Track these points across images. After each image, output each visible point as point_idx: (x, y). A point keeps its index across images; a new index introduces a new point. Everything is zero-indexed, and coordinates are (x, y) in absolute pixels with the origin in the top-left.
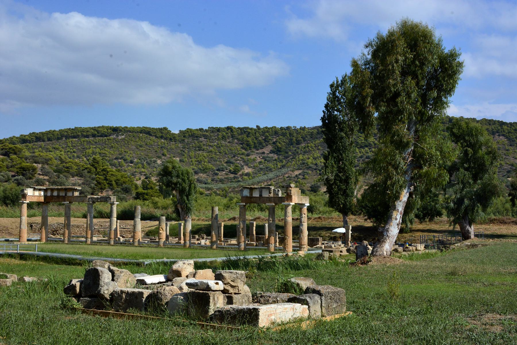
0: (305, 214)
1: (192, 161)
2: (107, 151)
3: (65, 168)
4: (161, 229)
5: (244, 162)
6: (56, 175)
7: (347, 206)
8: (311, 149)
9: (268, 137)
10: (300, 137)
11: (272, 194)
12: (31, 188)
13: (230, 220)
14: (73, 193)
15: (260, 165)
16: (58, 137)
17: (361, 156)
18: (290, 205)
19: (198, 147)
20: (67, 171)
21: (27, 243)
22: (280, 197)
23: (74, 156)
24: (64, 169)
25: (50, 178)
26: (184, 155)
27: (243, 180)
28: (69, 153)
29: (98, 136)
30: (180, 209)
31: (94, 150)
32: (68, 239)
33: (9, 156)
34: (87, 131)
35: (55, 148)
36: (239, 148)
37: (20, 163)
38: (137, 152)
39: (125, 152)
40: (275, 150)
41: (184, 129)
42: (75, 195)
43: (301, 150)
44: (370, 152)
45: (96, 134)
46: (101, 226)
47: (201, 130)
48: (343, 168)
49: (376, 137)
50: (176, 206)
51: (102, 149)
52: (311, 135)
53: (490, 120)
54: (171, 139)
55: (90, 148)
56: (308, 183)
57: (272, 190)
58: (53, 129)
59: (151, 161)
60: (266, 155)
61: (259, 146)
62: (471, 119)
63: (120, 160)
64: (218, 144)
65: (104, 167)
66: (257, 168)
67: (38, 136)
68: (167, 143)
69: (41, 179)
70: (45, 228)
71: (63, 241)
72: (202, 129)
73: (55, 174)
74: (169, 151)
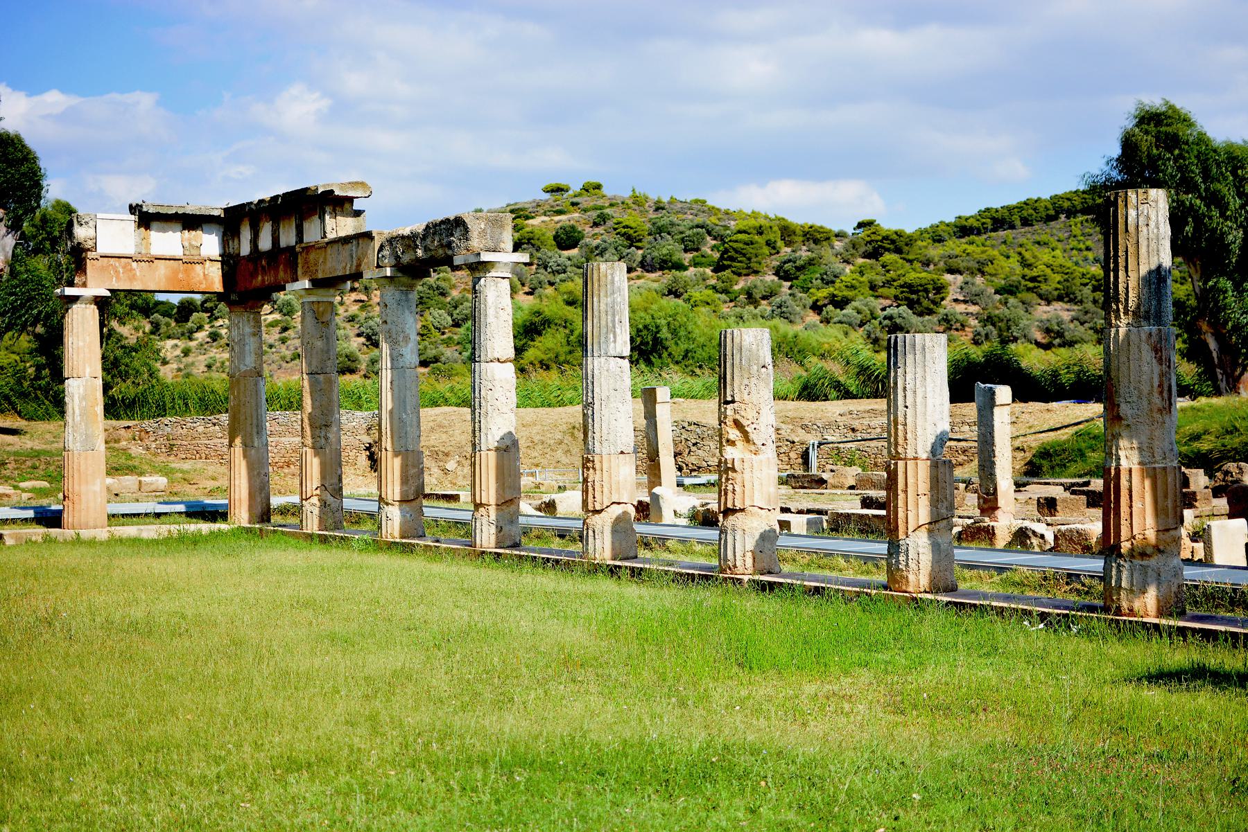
4: (733, 434)
6: (1000, 302)
20: (1035, 287)
23: (1086, 259)
24: (1023, 282)
35: (1039, 243)
46: (853, 430)
67: (998, 216)
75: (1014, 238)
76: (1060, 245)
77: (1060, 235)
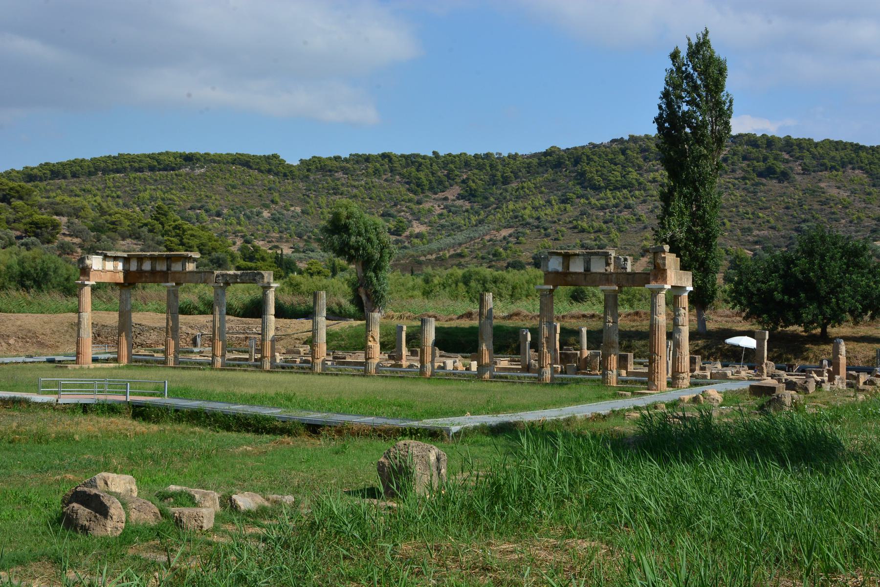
0: (684, 308)
1: (322, 213)
2: (175, 195)
3: (110, 223)
4: (371, 339)
5: (413, 214)
6: (94, 237)
7: (706, 291)
8: (527, 191)
9: (453, 171)
10: (509, 170)
11: (612, 266)
12: (97, 254)
13: (461, 317)
14: (184, 266)
15: (440, 219)
16: (89, 171)
17: (616, 204)
18: (662, 289)
19: (333, 189)
20: (113, 228)
21: (92, 366)
22: (629, 274)
24: (107, 225)
25: (84, 241)
26: (308, 203)
27: (413, 246)
28: (109, 198)
29: (160, 170)
30: (364, 298)
31: (154, 193)
32: (175, 357)
33: (9, 203)
34: (141, 161)
35: (84, 190)
36: (403, 189)
37: (31, 215)
38: (227, 197)
39: (207, 196)
40: (466, 194)
41: (307, 157)
42: (187, 270)
43: (511, 194)
44: (632, 196)
45: (155, 166)
47: (337, 158)
48: (702, 217)
49: (641, 172)
50: (356, 291)
51: (167, 192)
52: (528, 167)
53: (837, 142)
54: (285, 175)
55: (145, 190)
56: (526, 250)
57: (612, 257)
58: (80, 158)
59: (251, 212)
60: (449, 203)
61: (437, 186)
62: (805, 139)
63: (199, 211)
64: (367, 184)
65: (177, 223)
66: (435, 225)
68: (279, 182)
69: (69, 243)
70: (127, 336)
71: (164, 362)
72: (339, 157)
73: (93, 234)
74: (283, 195)
75: (66, 186)
76: (99, 193)
77: (99, 186)
